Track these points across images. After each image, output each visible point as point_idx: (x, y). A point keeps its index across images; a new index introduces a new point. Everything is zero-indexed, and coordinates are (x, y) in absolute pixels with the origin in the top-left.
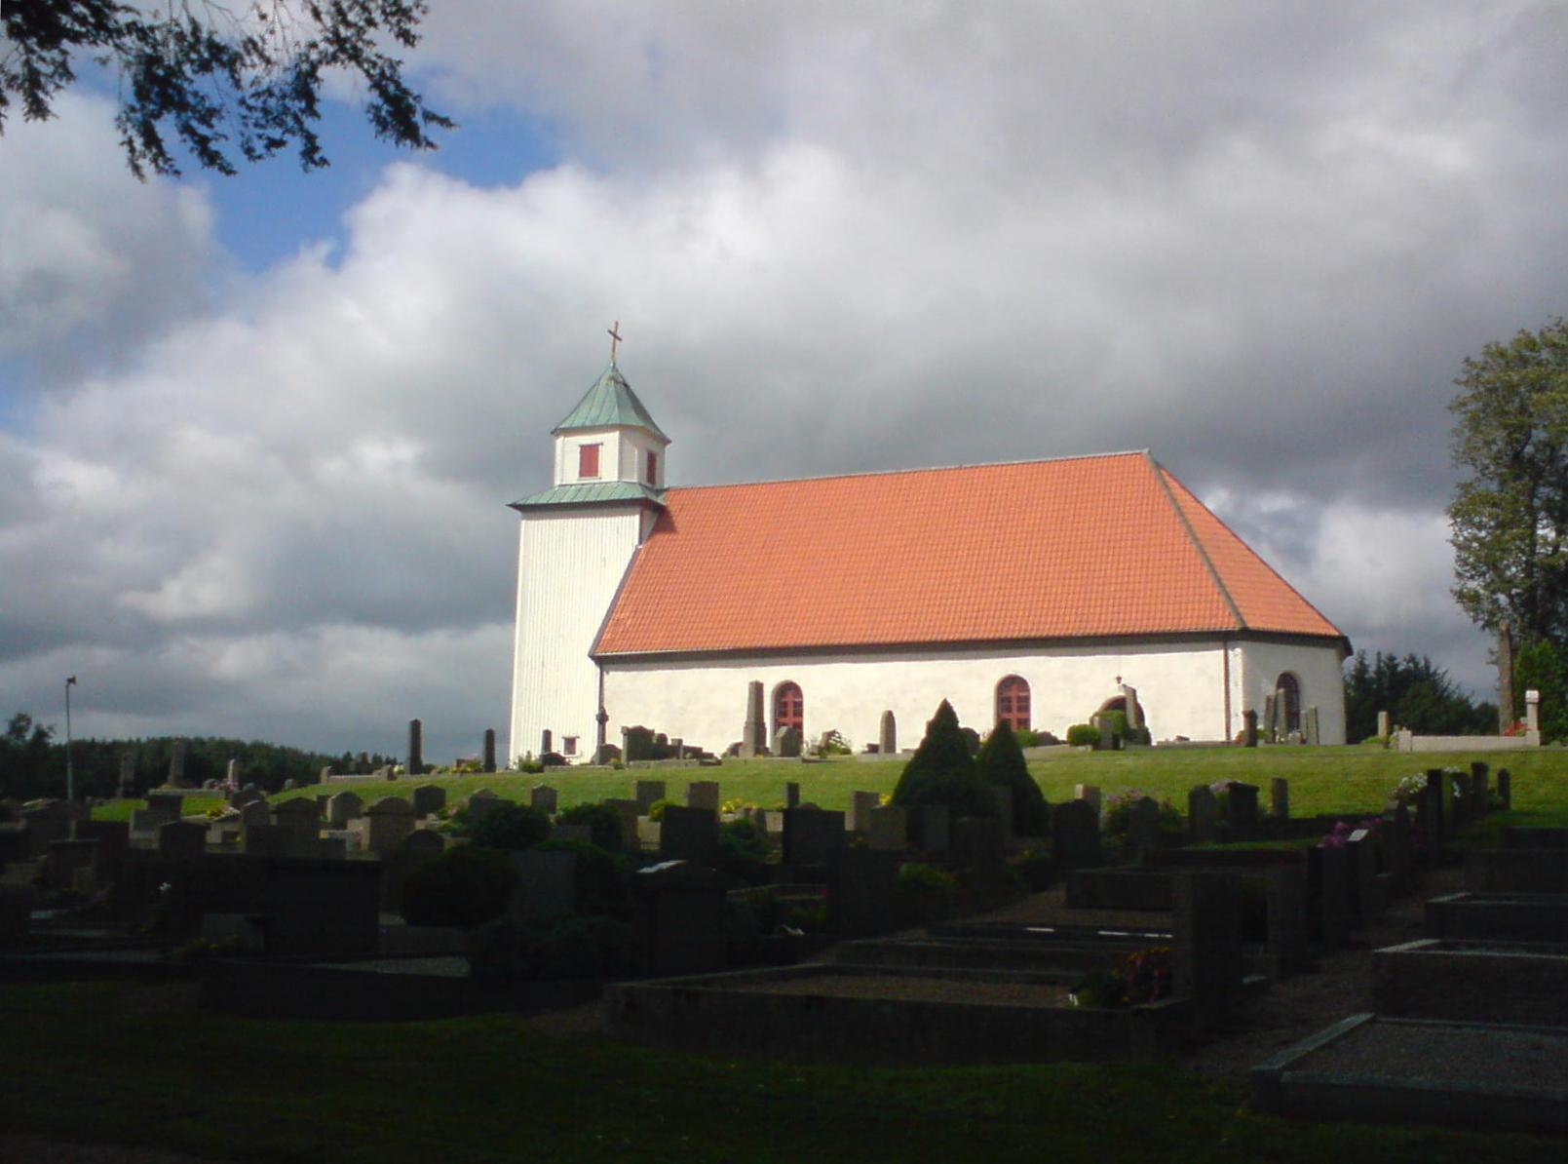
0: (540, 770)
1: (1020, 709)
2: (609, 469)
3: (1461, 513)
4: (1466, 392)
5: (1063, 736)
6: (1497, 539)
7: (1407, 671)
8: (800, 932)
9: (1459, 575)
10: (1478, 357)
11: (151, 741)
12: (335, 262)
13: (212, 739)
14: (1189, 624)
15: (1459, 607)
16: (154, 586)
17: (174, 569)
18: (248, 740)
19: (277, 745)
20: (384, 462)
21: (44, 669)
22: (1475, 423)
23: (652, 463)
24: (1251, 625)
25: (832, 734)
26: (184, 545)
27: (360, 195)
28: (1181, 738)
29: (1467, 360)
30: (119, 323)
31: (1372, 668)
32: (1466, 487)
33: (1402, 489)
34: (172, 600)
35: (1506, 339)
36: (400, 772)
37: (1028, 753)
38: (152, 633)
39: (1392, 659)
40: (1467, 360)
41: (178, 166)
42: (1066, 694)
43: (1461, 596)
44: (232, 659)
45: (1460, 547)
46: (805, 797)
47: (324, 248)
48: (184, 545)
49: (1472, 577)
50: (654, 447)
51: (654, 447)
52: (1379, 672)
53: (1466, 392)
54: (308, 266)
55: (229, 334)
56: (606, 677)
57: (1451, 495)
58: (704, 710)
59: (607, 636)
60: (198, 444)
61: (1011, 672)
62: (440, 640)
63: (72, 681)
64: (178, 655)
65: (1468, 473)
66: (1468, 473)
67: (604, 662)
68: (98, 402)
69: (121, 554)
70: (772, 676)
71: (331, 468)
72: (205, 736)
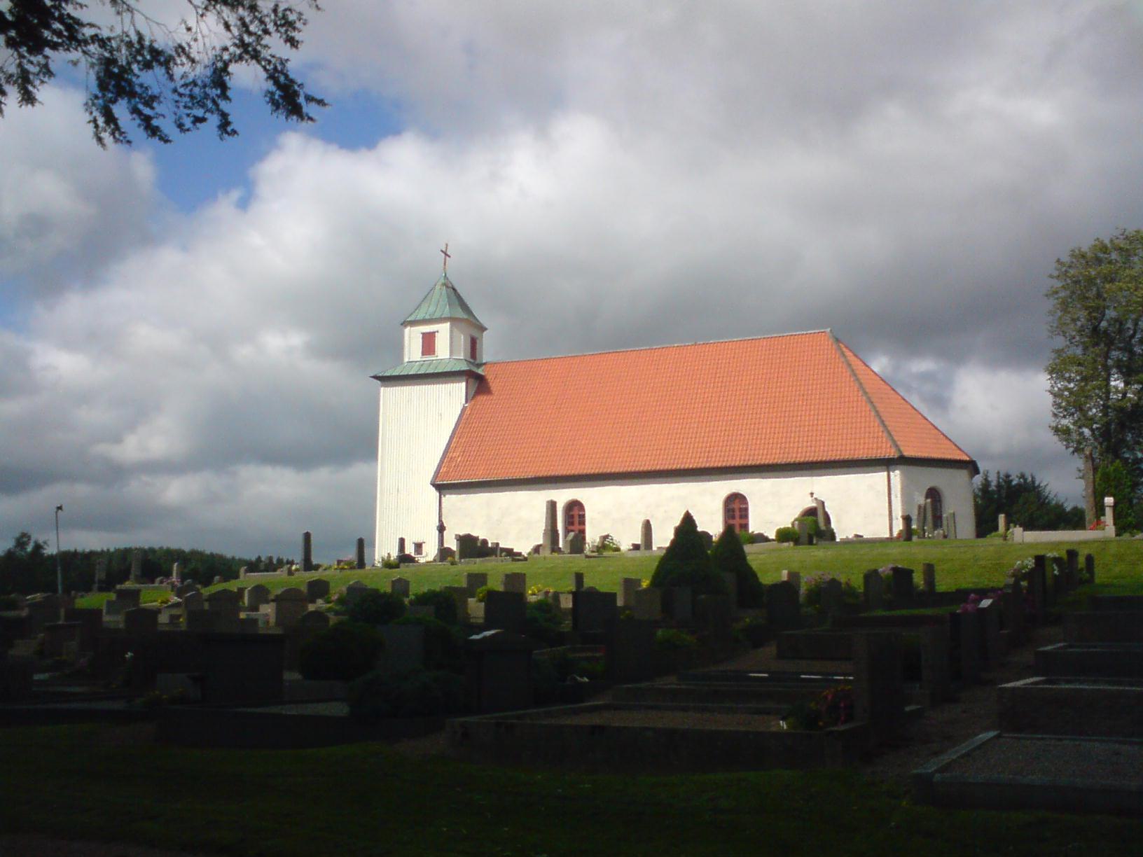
0: (397, 566)
1: (741, 517)
2: (443, 349)
3: (1056, 371)
4: (1058, 284)
5: (772, 536)
6: (1082, 389)
7: (1019, 485)
8: (586, 680)
9: (1055, 415)
10: (1066, 259)
11: (117, 551)
12: (244, 204)
13: (161, 548)
14: (862, 454)
15: (1056, 438)
16: (118, 440)
17: (132, 427)
18: (187, 549)
19: (208, 552)
20: (281, 347)
21: (40, 500)
22: (1065, 306)
23: (474, 345)
24: (908, 453)
25: (607, 537)
26: (138, 410)
27: (261, 156)
28: (857, 536)
29: (1058, 261)
30: (89, 250)
31: (994, 483)
32: (1059, 352)
33: (1012, 354)
34: (131, 449)
35: (1086, 245)
36: (297, 570)
37: (747, 548)
38: (117, 473)
39: (1008, 476)
40: (1058, 261)
41: (130, 137)
42: (774, 505)
43: (1057, 430)
44: (175, 491)
45: (1055, 395)
46: (588, 583)
47: (236, 194)
48: (138, 410)
49: (1064, 417)
50: (476, 334)
51: (476, 334)
52: (999, 486)
53: (1058, 284)
54: (224, 207)
55: (168, 258)
56: (443, 499)
57: (1048, 358)
58: (514, 521)
59: (443, 470)
60: (148, 337)
61: (734, 491)
62: (323, 474)
63: (60, 508)
64: (135, 488)
65: (1060, 342)
66: (1060, 342)
67: (442, 488)
68: (75, 308)
69: (93, 417)
70: (563, 496)
71: (244, 353)
72: (156, 547)
